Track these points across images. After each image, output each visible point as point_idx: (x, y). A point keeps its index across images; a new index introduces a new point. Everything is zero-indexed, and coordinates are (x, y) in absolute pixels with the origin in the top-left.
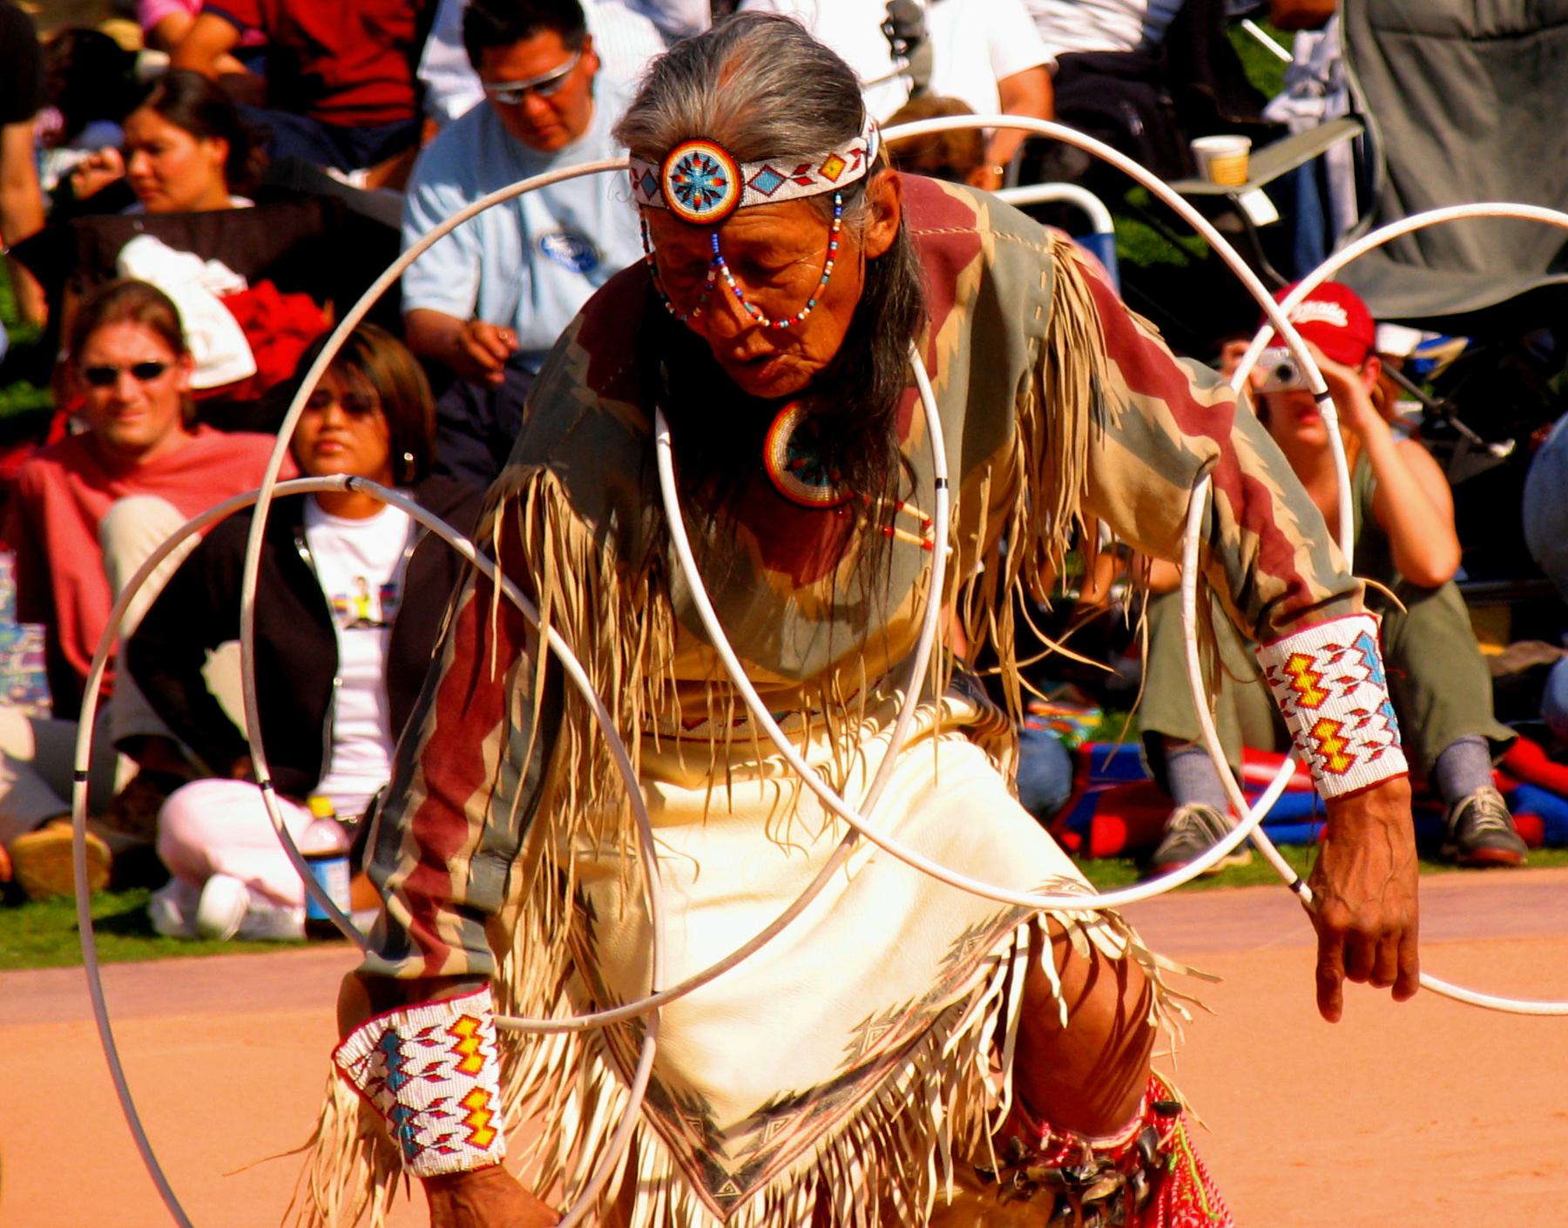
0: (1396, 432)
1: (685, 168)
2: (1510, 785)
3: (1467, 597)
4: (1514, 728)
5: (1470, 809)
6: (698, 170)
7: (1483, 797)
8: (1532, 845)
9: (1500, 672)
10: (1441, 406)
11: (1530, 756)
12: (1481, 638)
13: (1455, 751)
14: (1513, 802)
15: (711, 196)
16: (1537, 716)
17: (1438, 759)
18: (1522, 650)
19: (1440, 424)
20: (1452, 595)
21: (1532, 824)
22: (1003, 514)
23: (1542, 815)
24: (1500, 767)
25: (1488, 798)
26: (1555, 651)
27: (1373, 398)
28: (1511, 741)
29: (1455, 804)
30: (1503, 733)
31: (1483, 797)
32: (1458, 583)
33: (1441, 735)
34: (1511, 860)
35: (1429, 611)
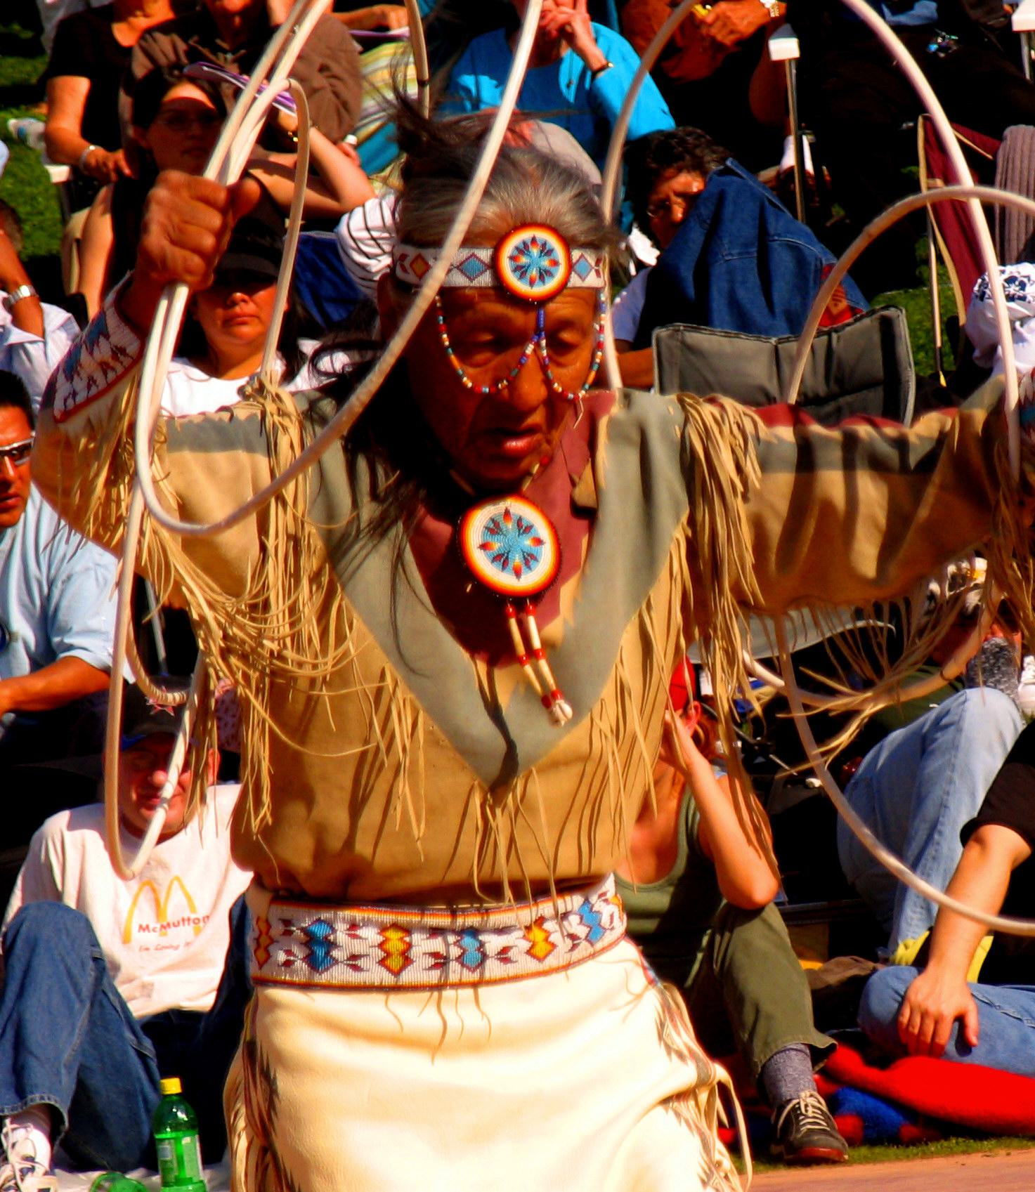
0: (717, 768)
1: (523, 249)
2: (832, 1088)
3: (786, 916)
4: (833, 1036)
5: (796, 1109)
6: (535, 251)
7: (805, 1096)
8: (852, 1143)
9: (819, 985)
10: (759, 744)
11: (849, 1060)
12: (801, 955)
13: (779, 1059)
14: (834, 1104)
15: (544, 275)
16: (856, 1025)
17: (764, 1067)
18: (838, 964)
19: (760, 760)
20: (773, 916)
21: (852, 1123)
22: (961, 344)
23: (860, 1115)
24: (821, 1072)
25: (811, 1101)
26: (871, 965)
27: (695, 737)
28: (832, 1047)
29: (782, 1107)
30: (823, 1041)
31: (805, 1096)
32: (777, 904)
33: (766, 1044)
34: (834, 1156)
35: (752, 932)
